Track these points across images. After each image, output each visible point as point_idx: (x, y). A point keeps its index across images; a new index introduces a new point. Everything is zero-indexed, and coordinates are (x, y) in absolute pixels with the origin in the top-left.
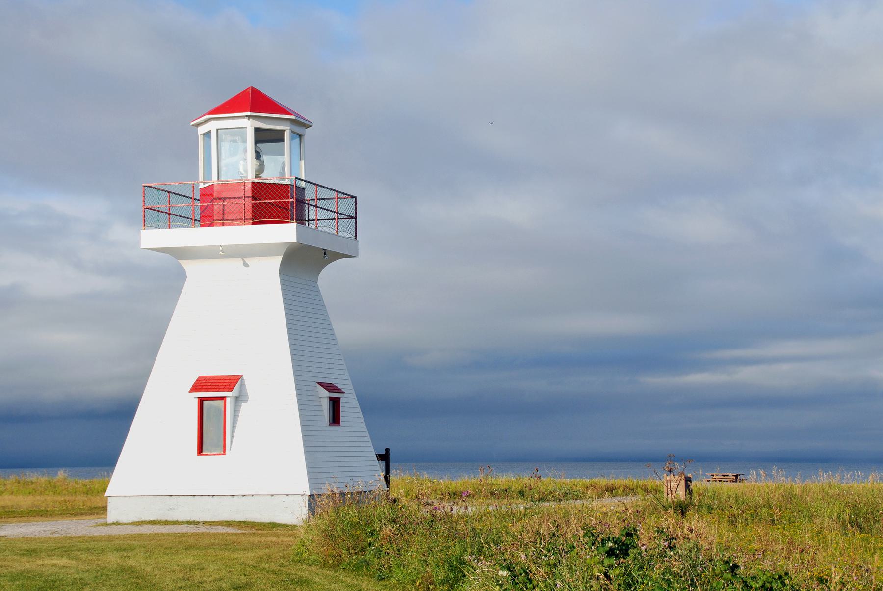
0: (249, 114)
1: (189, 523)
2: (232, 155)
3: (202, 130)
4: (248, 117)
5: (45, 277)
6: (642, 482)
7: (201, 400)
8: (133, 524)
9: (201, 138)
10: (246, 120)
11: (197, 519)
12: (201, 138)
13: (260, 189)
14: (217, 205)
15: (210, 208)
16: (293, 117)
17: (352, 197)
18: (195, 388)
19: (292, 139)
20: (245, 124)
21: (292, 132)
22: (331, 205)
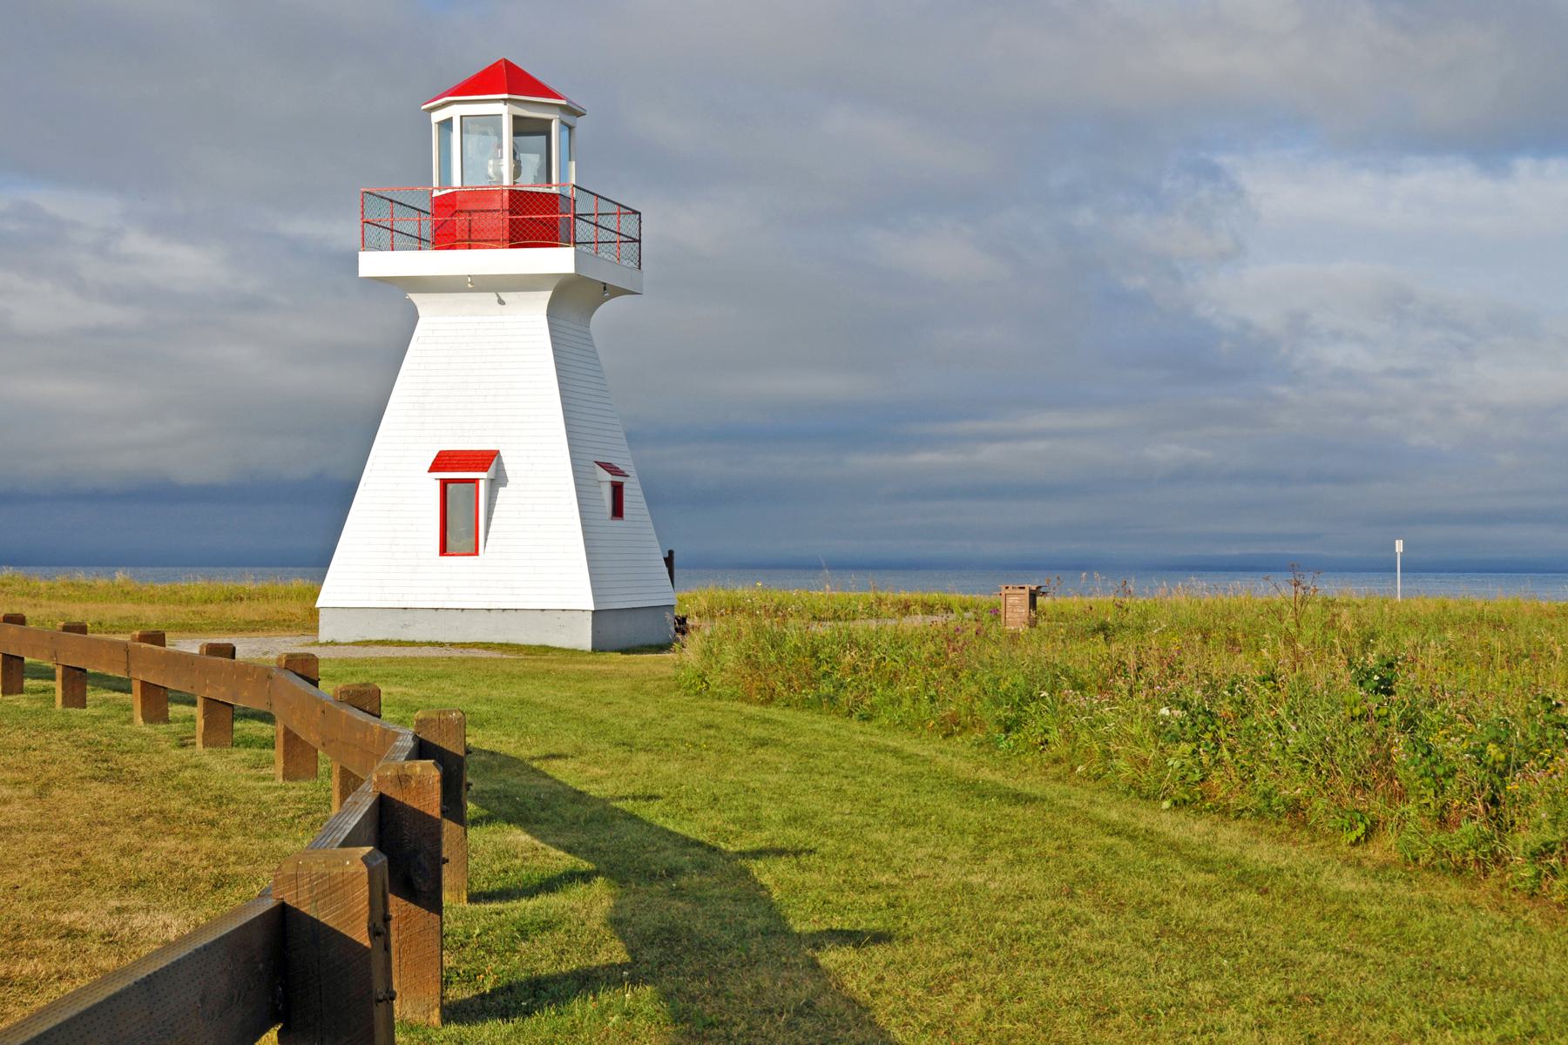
0: (505, 96)
1: (430, 644)
2: (480, 149)
3: (437, 117)
4: (505, 101)
5: (39, 305)
6: (919, 596)
7: (444, 483)
8: (355, 644)
9: (435, 129)
10: (501, 105)
11: (441, 640)
12: (435, 129)
13: (518, 199)
14: (461, 220)
15: (452, 223)
16: (563, 102)
17: (635, 212)
18: (435, 467)
19: (561, 131)
20: (499, 108)
21: (562, 122)
22: (611, 222)
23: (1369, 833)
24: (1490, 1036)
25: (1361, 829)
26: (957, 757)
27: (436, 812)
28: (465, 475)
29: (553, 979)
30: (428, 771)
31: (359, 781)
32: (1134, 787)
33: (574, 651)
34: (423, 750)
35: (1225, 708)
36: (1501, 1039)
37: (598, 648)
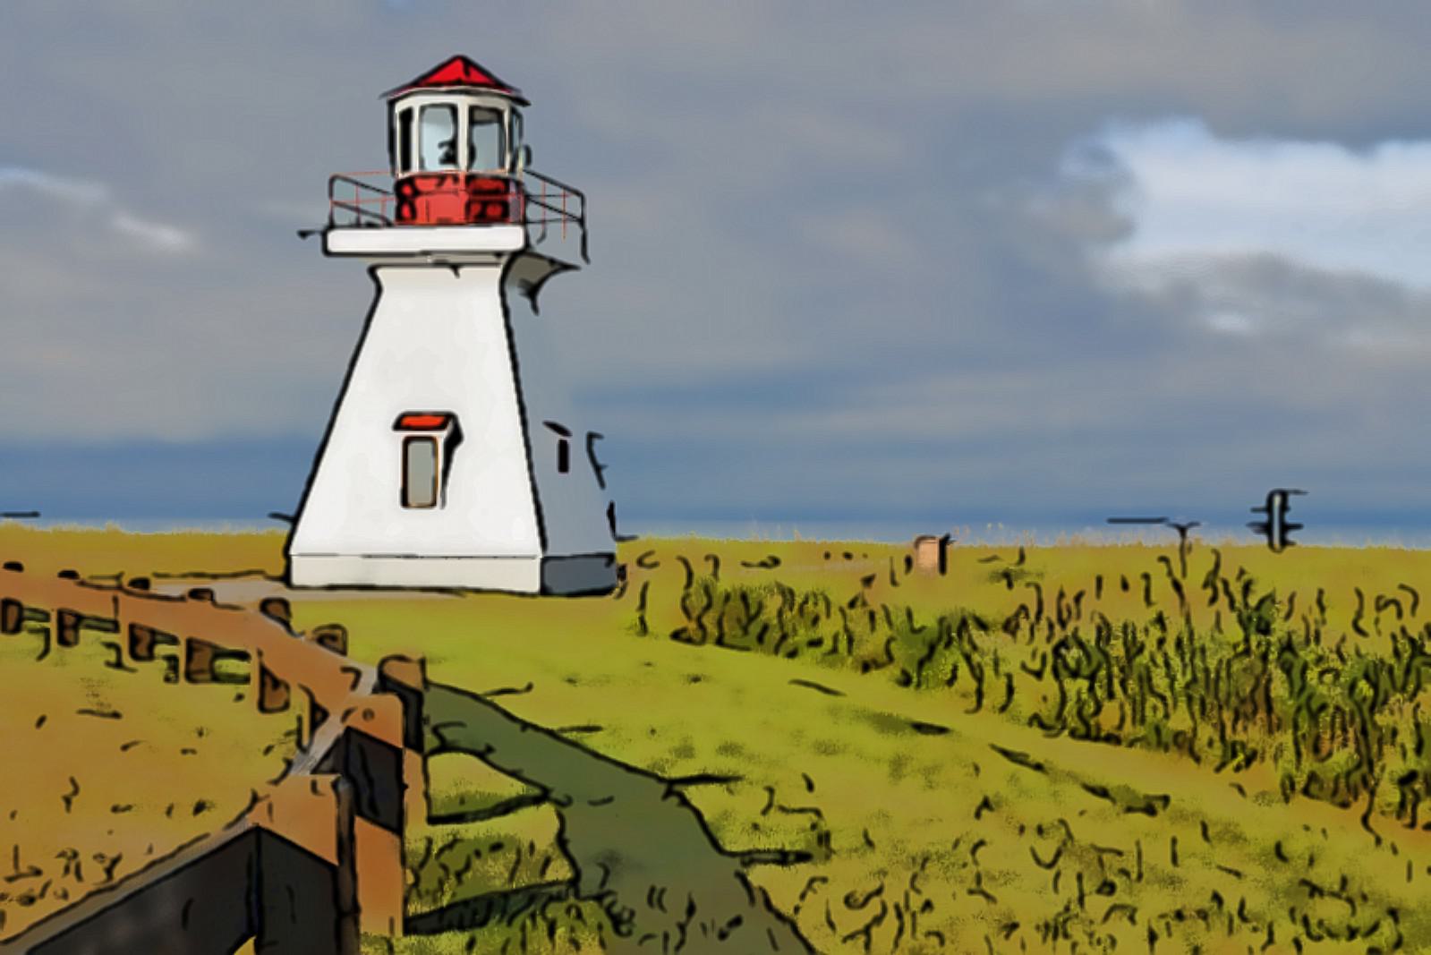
7: (407, 441)
17: (577, 193)
18: (398, 426)
23: (1249, 761)
24: (1361, 945)
25: (1241, 757)
26: (880, 691)
27: (401, 746)
28: (431, 434)
29: (505, 895)
30: (391, 706)
31: (325, 715)
32: (1036, 720)
33: (522, 594)
34: (385, 684)
35: (1117, 649)
36: (1371, 950)
37: (545, 591)
